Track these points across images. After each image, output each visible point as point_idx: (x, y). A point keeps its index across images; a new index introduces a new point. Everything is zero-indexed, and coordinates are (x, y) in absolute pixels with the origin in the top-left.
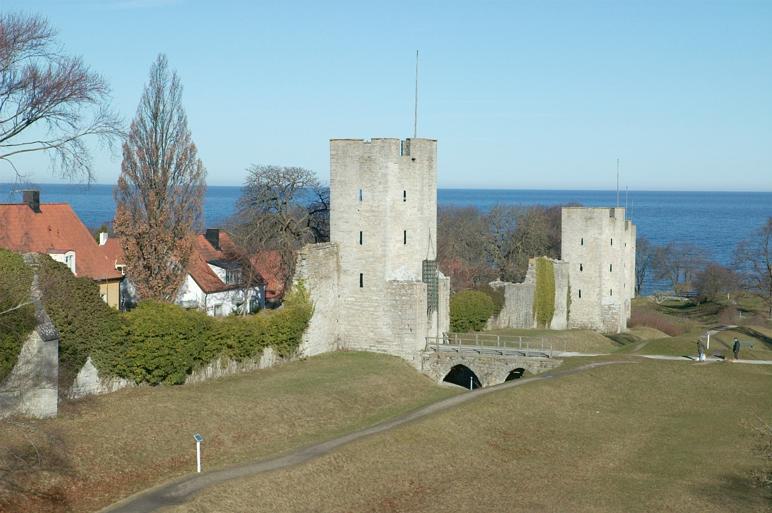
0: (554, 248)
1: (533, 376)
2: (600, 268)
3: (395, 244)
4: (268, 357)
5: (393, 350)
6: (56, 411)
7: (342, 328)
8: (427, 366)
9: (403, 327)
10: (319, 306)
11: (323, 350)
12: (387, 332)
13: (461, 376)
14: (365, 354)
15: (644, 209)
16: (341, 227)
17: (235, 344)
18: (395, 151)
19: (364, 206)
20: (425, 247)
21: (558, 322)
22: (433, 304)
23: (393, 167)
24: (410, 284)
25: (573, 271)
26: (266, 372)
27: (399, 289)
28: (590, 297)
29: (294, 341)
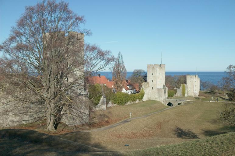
4: (138, 101)
5: (158, 100)
7: (149, 96)
9: (160, 96)
10: (145, 92)
11: (146, 100)
12: (157, 97)
13: (170, 104)
14: (153, 101)
15: (200, 75)
16: (149, 79)
17: (132, 98)
18: (158, 67)
19: (153, 76)
20: (163, 82)
21: (186, 95)
25: (189, 86)
26: (137, 103)
27: (159, 90)
29: (142, 98)
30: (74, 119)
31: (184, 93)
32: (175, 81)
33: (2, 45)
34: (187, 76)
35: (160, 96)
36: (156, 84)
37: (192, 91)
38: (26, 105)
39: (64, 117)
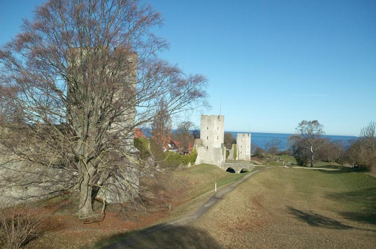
0: (235, 142)
1: (250, 172)
2: (246, 147)
3: (215, 139)
4: (189, 165)
5: (214, 164)
6: (173, 129)
7: (203, 159)
8: (222, 168)
9: (217, 158)
10: (199, 153)
11: (199, 163)
12: (213, 159)
13: (230, 170)
14: (208, 165)
15: (255, 136)
16: (203, 136)
17: (184, 161)
18: (216, 118)
19: (209, 130)
20: (222, 141)
21: (237, 159)
22: (223, 154)
23: (215, 122)
24: (219, 149)
25: (240, 148)
26: (190, 168)
27: (216, 150)
28: (243, 153)
29: (194, 161)
30: (119, 194)
31: (235, 156)
32: (230, 140)
33: (3, 50)
34: (238, 134)
35: (217, 158)
36: (213, 142)
37: (244, 153)
38: (38, 169)
39: (102, 189)
